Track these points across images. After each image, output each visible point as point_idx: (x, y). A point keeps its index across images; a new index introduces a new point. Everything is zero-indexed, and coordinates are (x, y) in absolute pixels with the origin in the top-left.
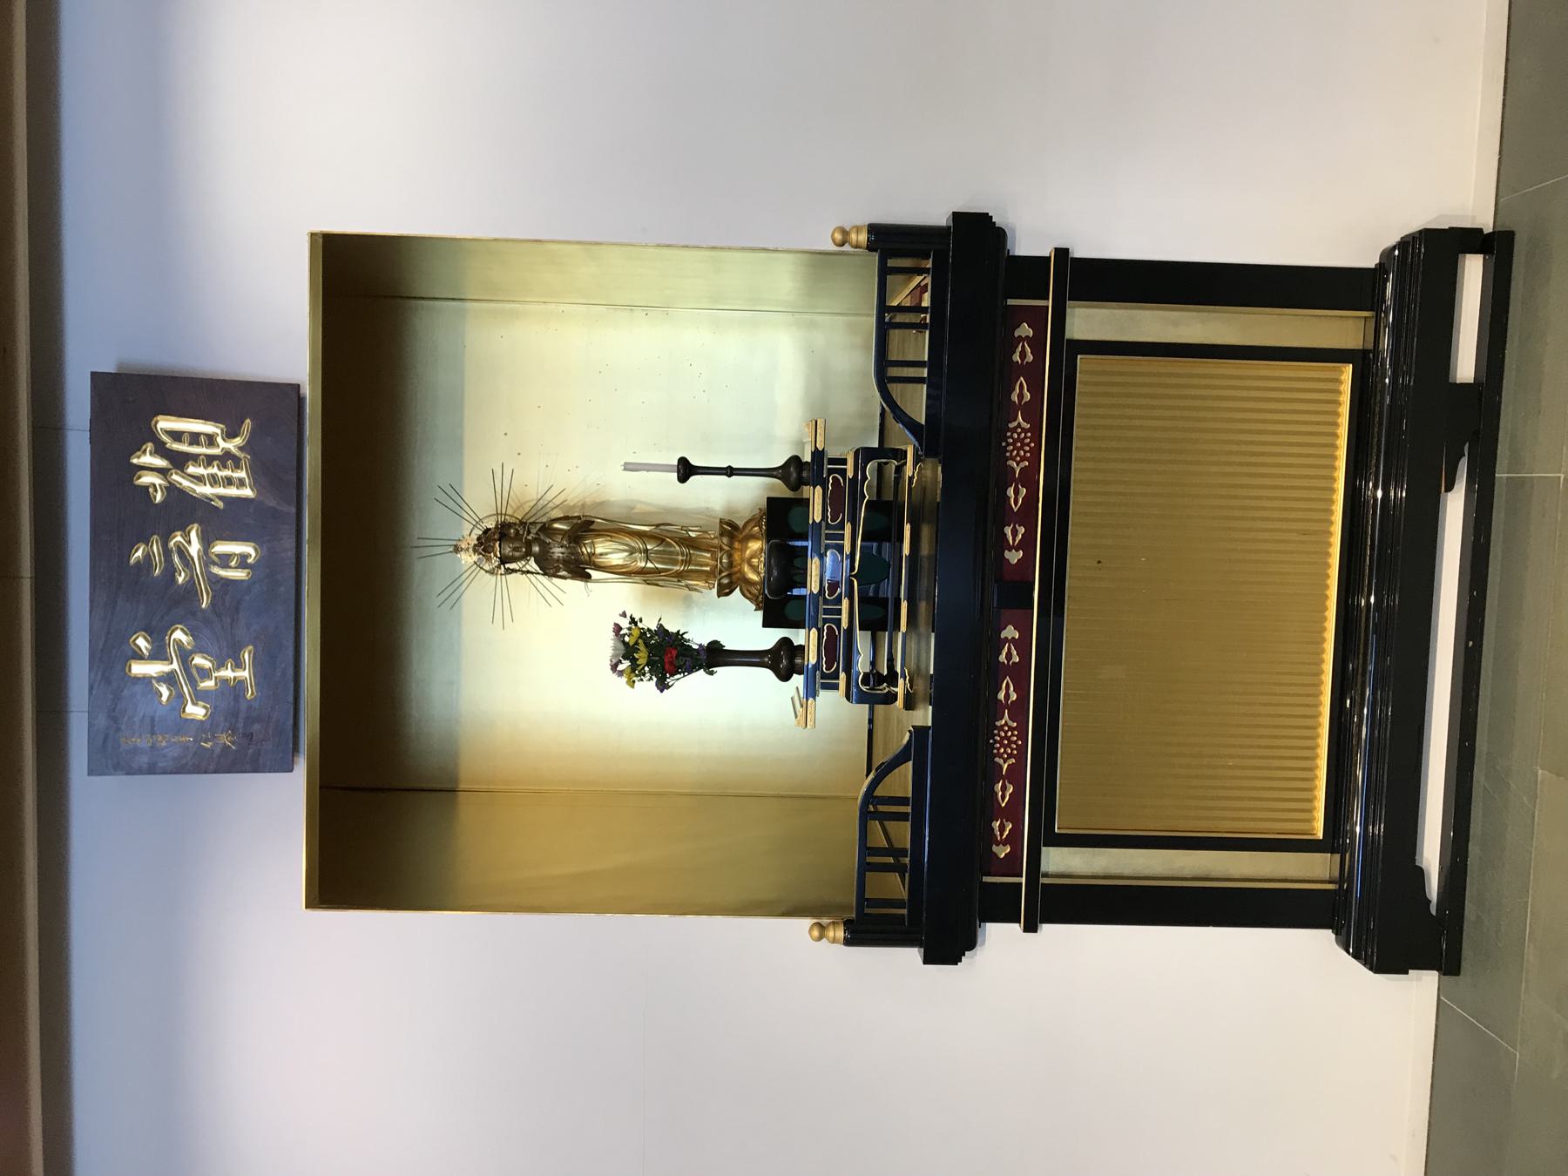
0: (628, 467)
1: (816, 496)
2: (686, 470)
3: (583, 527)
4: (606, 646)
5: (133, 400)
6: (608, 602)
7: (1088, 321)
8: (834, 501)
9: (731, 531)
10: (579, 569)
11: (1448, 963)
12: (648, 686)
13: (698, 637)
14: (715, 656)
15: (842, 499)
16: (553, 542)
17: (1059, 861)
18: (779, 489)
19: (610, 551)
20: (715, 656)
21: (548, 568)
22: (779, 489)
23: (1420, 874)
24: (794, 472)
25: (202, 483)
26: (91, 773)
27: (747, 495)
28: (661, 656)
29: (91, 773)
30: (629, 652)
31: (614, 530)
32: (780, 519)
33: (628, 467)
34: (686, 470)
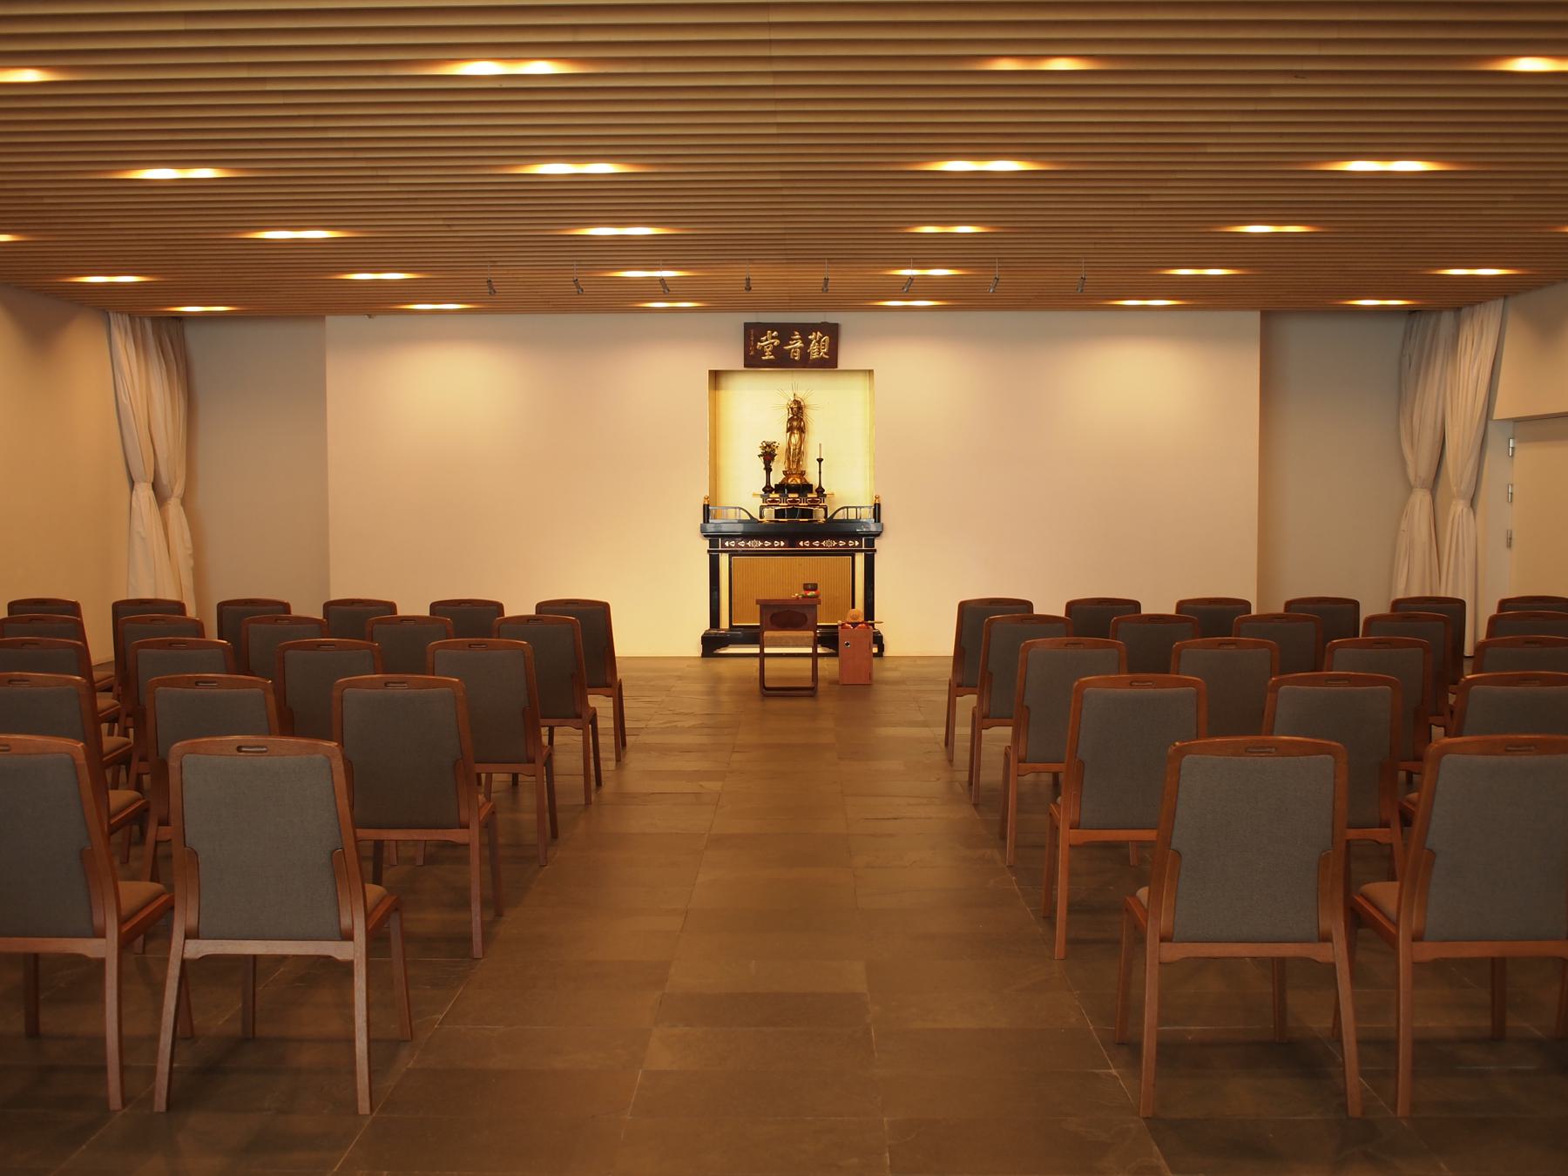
0: (1509, 545)
1: (814, 495)
2: (820, 460)
3: (802, 430)
4: (769, 440)
5: (832, 331)
6: (778, 435)
7: (860, 559)
8: (813, 500)
9: (802, 474)
10: (790, 430)
11: (704, 655)
12: (760, 452)
13: (773, 465)
14: (768, 470)
15: (814, 502)
16: (797, 419)
17: (724, 559)
18: (816, 485)
19: (795, 438)
20: (768, 470)
21: (790, 420)
22: (816, 485)
23: (726, 646)
24: (820, 491)
25: (813, 347)
26: (746, 325)
27: (813, 479)
28: (768, 455)
29: (746, 325)
30: (769, 446)
31: (801, 440)
32: (805, 488)
33: (1509, 545)
34: (820, 460)
